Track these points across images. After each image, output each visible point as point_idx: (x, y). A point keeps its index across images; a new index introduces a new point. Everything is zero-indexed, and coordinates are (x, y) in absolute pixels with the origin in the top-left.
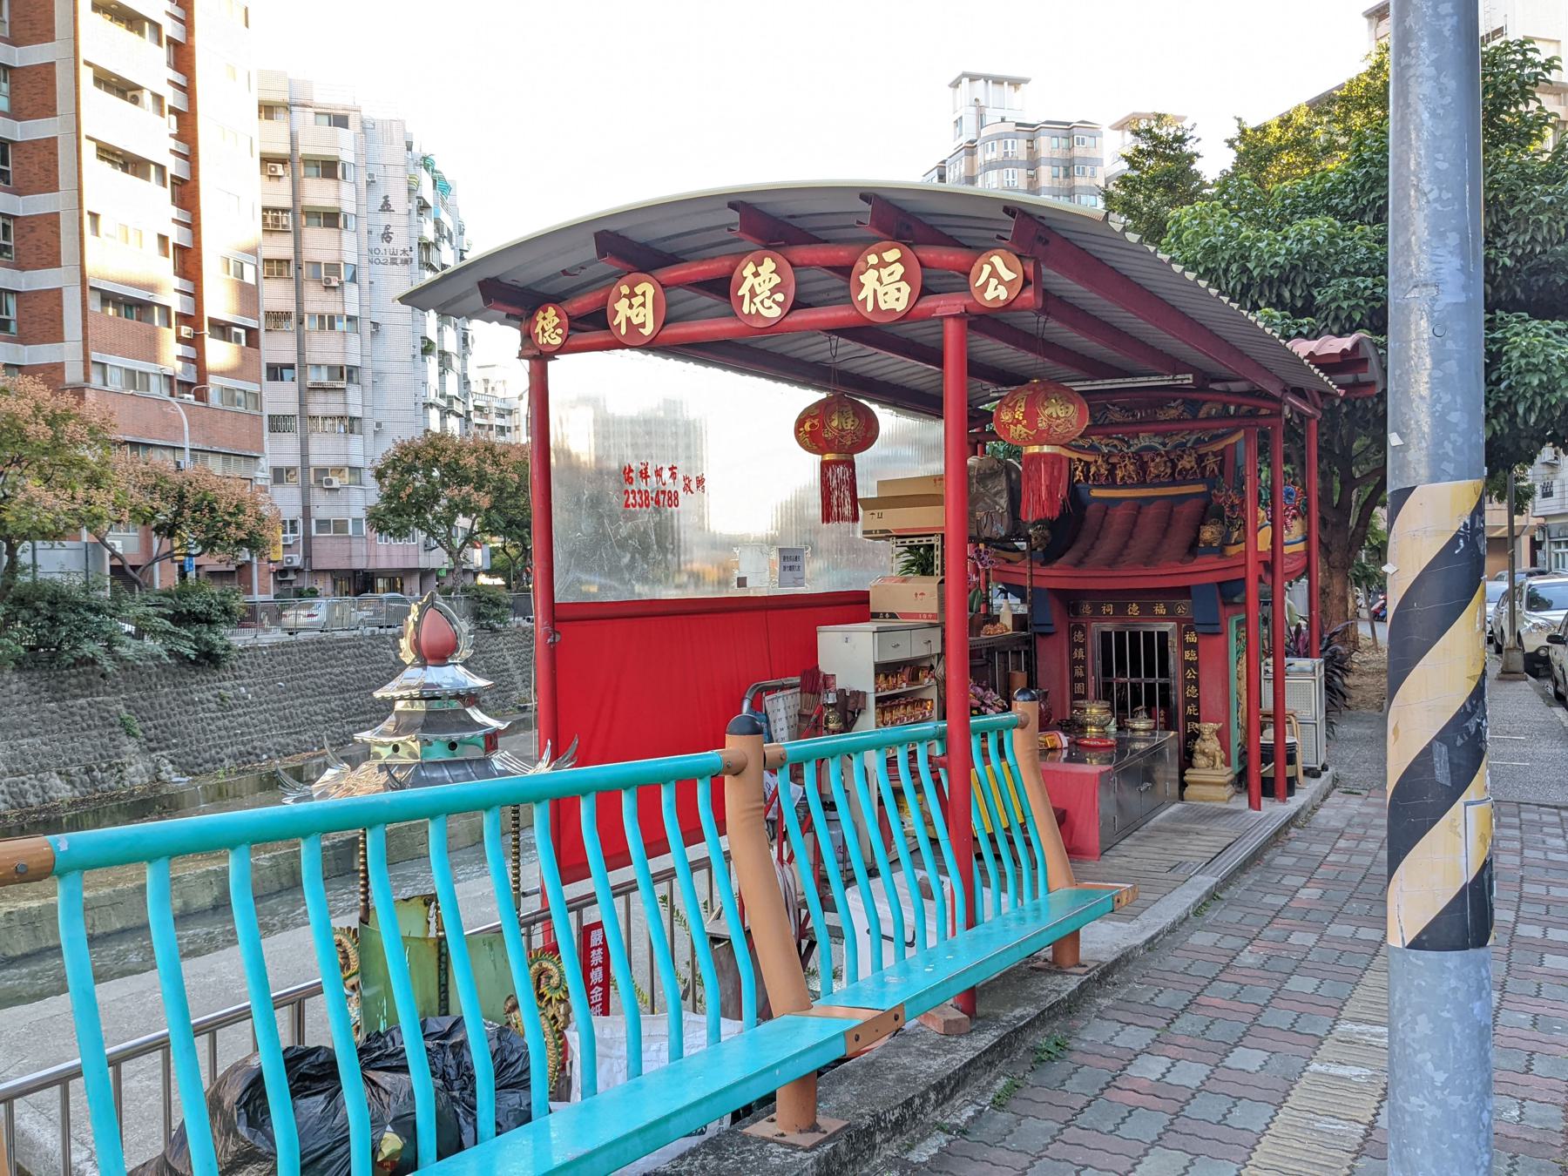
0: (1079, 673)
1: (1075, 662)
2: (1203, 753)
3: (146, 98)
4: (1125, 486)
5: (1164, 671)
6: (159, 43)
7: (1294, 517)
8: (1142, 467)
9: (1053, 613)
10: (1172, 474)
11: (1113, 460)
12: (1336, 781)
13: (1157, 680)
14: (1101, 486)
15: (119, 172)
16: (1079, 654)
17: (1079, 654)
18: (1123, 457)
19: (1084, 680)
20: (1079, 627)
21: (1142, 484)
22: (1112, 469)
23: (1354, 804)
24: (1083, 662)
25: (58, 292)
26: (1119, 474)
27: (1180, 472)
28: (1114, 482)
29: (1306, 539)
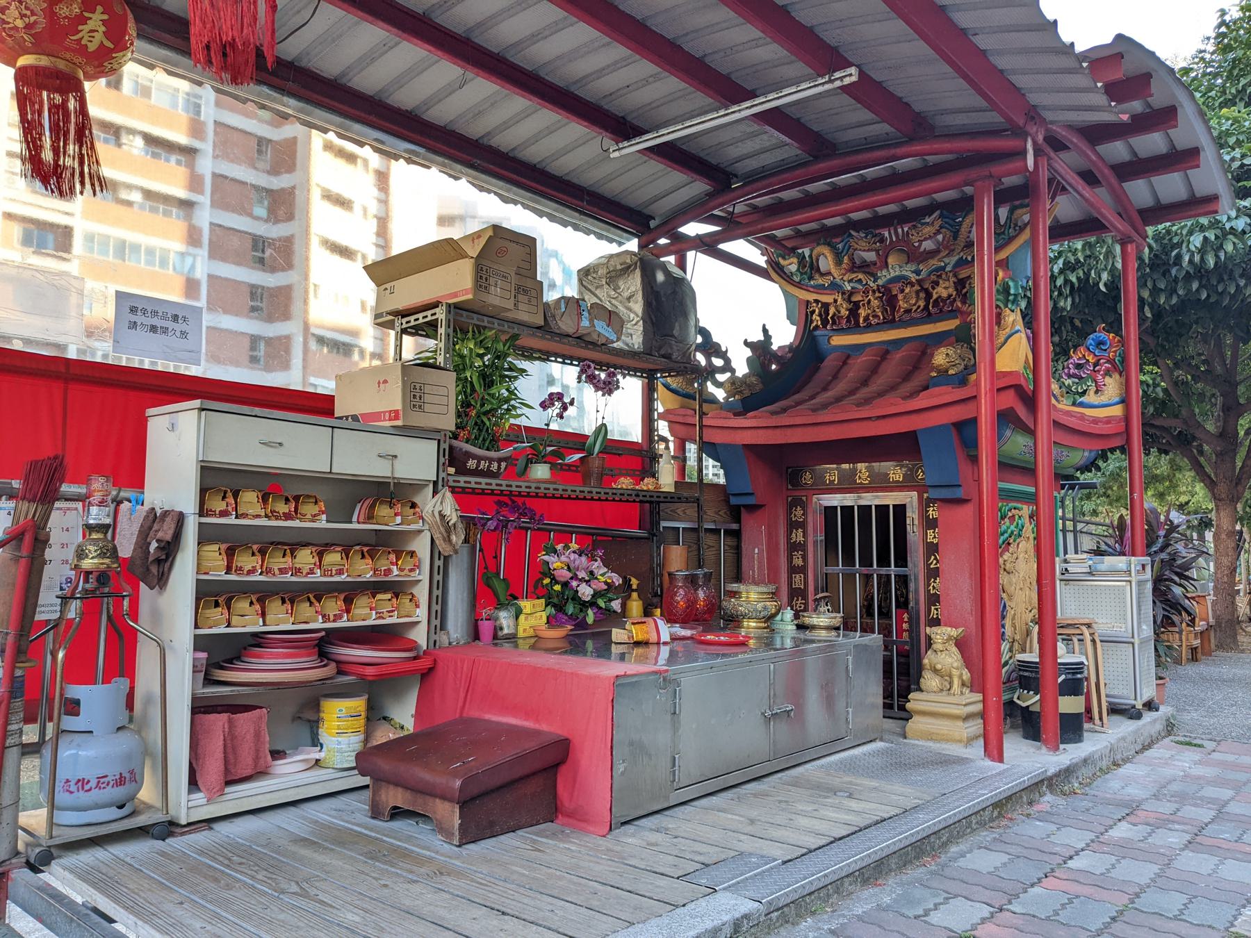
0: (798, 562)
1: (793, 547)
2: (936, 671)
3: (357, 207)
4: (869, 327)
5: (902, 560)
6: (367, 170)
7: (1107, 373)
8: (890, 301)
9: (755, 482)
10: (926, 307)
11: (855, 298)
12: (1170, 728)
13: (893, 570)
14: (841, 331)
15: (328, 252)
16: (798, 536)
17: (798, 536)
18: (866, 292)
19: (803, 570)
20: (797, 502)
21: (890, 323)
22: (854, 312)
23: (1186, 761)
24: (802, 547)
25: (288, 338)
26: (863, 312)
27: (936, 302)
28: (857, 324)
29: (1125, 401)
